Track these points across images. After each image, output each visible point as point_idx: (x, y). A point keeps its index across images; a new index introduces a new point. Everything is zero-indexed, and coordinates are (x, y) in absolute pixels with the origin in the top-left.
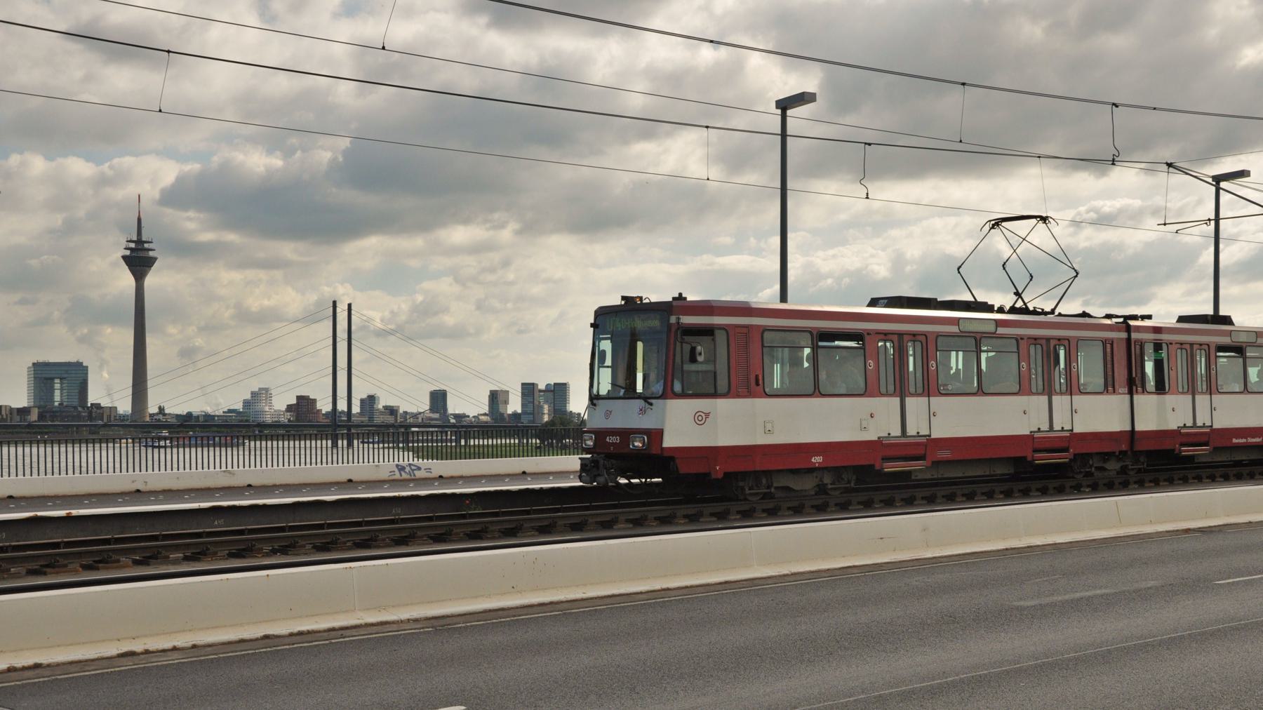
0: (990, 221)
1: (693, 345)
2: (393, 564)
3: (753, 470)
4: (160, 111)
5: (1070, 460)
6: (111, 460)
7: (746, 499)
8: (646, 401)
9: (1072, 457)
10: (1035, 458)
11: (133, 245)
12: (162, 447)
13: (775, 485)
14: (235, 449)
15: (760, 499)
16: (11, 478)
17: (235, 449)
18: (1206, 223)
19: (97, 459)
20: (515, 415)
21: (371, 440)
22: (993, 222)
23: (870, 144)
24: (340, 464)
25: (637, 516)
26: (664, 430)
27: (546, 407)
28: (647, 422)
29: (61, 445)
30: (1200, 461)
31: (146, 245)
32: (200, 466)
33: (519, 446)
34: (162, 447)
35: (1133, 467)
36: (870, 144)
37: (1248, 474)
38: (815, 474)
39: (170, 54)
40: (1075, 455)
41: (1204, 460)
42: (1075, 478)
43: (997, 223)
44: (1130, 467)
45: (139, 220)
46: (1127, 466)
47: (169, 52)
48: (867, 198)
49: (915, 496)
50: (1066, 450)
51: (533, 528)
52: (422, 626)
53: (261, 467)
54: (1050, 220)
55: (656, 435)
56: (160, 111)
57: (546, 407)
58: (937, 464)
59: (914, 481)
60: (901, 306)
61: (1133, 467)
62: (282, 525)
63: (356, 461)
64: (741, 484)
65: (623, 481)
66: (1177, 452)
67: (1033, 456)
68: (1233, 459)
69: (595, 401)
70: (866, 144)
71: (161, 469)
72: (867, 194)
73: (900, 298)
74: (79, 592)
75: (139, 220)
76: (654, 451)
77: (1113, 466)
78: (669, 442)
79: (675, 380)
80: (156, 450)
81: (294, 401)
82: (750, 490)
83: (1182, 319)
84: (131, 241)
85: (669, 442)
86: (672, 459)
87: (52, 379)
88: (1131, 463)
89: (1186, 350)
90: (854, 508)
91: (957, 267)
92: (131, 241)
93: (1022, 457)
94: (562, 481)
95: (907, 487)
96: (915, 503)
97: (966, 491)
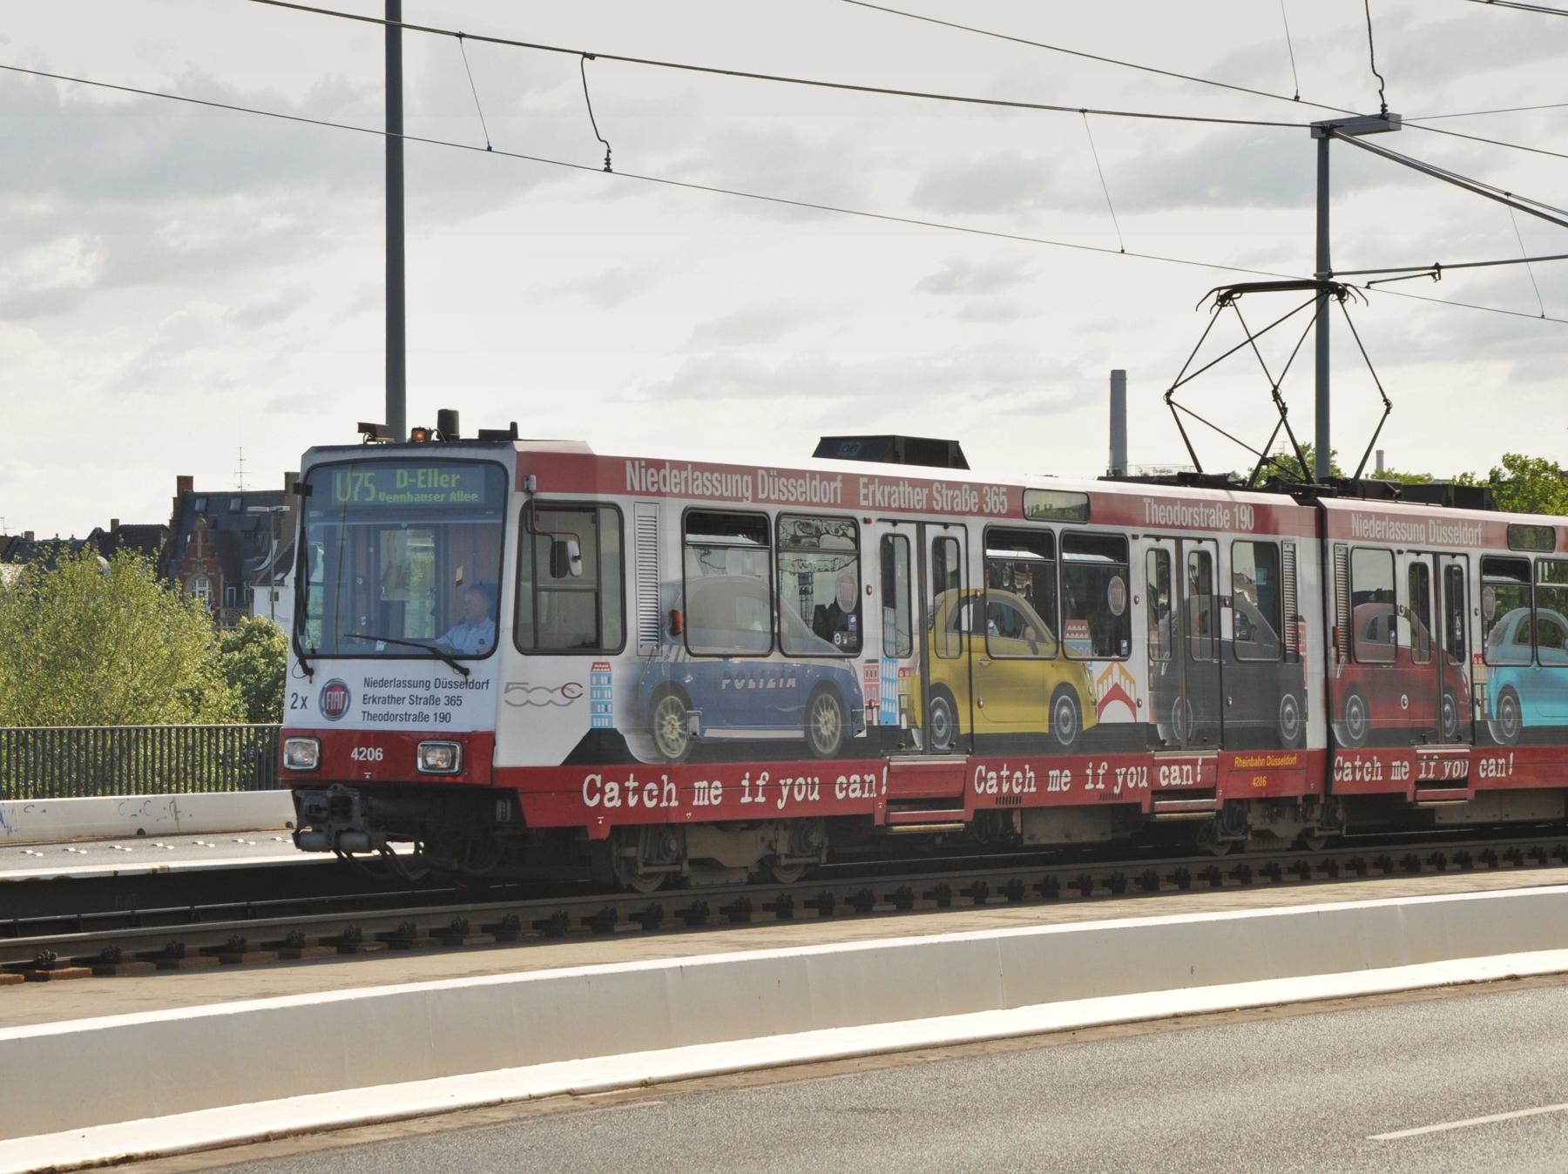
0: (1219, 289)
1: (557, 538)
2: (1327, 912)
3: (664, 821)
4: (489, 149)
5: (1470, 801)
7: (631, 889)
8: (455, 666)
9: (970, 818)
10: (892, 821)
13: (693, 854)
15: (658, 890)
18: (1433, 275)
22: (1223, 292)
25: (444, 923)
26: (497, 733)
28: (463, 721)
29: (969, 731)
30: (1443, 822)
35: (1322, 833)
37: (1402, 863)
38: (759, 833)
39: (463, 39)
40: (1227, 802)
41: (1456, 820)
42: (777, 882)
43: (1227, 296)
44: (1317, 833)
46: (1312, 829)
47: (461, 36)
48: (608, 170)
49: (613, 912)
50: (955, 802)
51: (324, 942)
52: (514, 1115)
54: (1349, 288)
55: (480, 744)
56: (489, 149)
58: (1483, 795)
59: (1029, 848)
60: (895, 459)
61: (1322, 833)
62: (9, 920)
64: (630, 852)
65: (404, 849)
66: (879, 820)
67: (1153, 805)
68: (1505, 819)
69: (309, 663)
72: (608, 160)
73: (892, 440)
74: (1541, 893)
76: (478, 777)
77: (1286, 829)
78: (507, 756)
79: (751, 628)
82: (645, 865)
83: (830, 447)
85: (507, 756)
86: (511, 795)
88: (1319, 825)
89: (955, 540)
90: (476, 940)
91: (1391, 411)
93: (1291, 798)
95: (1011, 862)
96: (988, 900)
97: (493, 920)
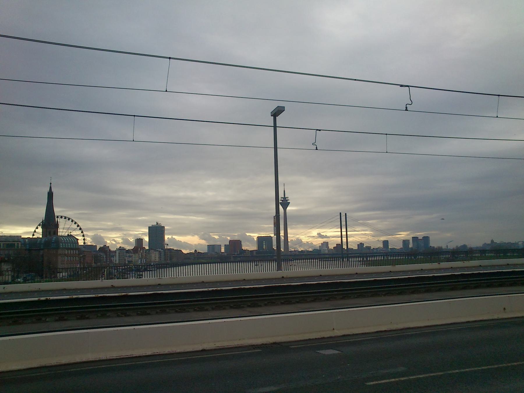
6: (212, 268)
11: (282, 199)
12: (151, 271)
14: (285, 262)
16: (131, 279)
17: (285, 262)
19: (221, 267)
20: (412, 248)
21: (330, 260)
23: (320, 130)
24: (353, 268)
27: (238, 259)
31: (286, 199)
32: (267, 271)
33: (416, 261)
34: (151, 271)
36: (320, 130)
45: (284, 191)
48: (317, 149)
53: (257, 272)
57: (238, 259)
63: (343, 267)
70: (317, 130)
71: (205, 274)
75: (284, 191)
80: (148, 272)
81: (335, 246)
84: (282, 198)
87: (263, 241)
92: (282, 198)
94: (201, 314)
